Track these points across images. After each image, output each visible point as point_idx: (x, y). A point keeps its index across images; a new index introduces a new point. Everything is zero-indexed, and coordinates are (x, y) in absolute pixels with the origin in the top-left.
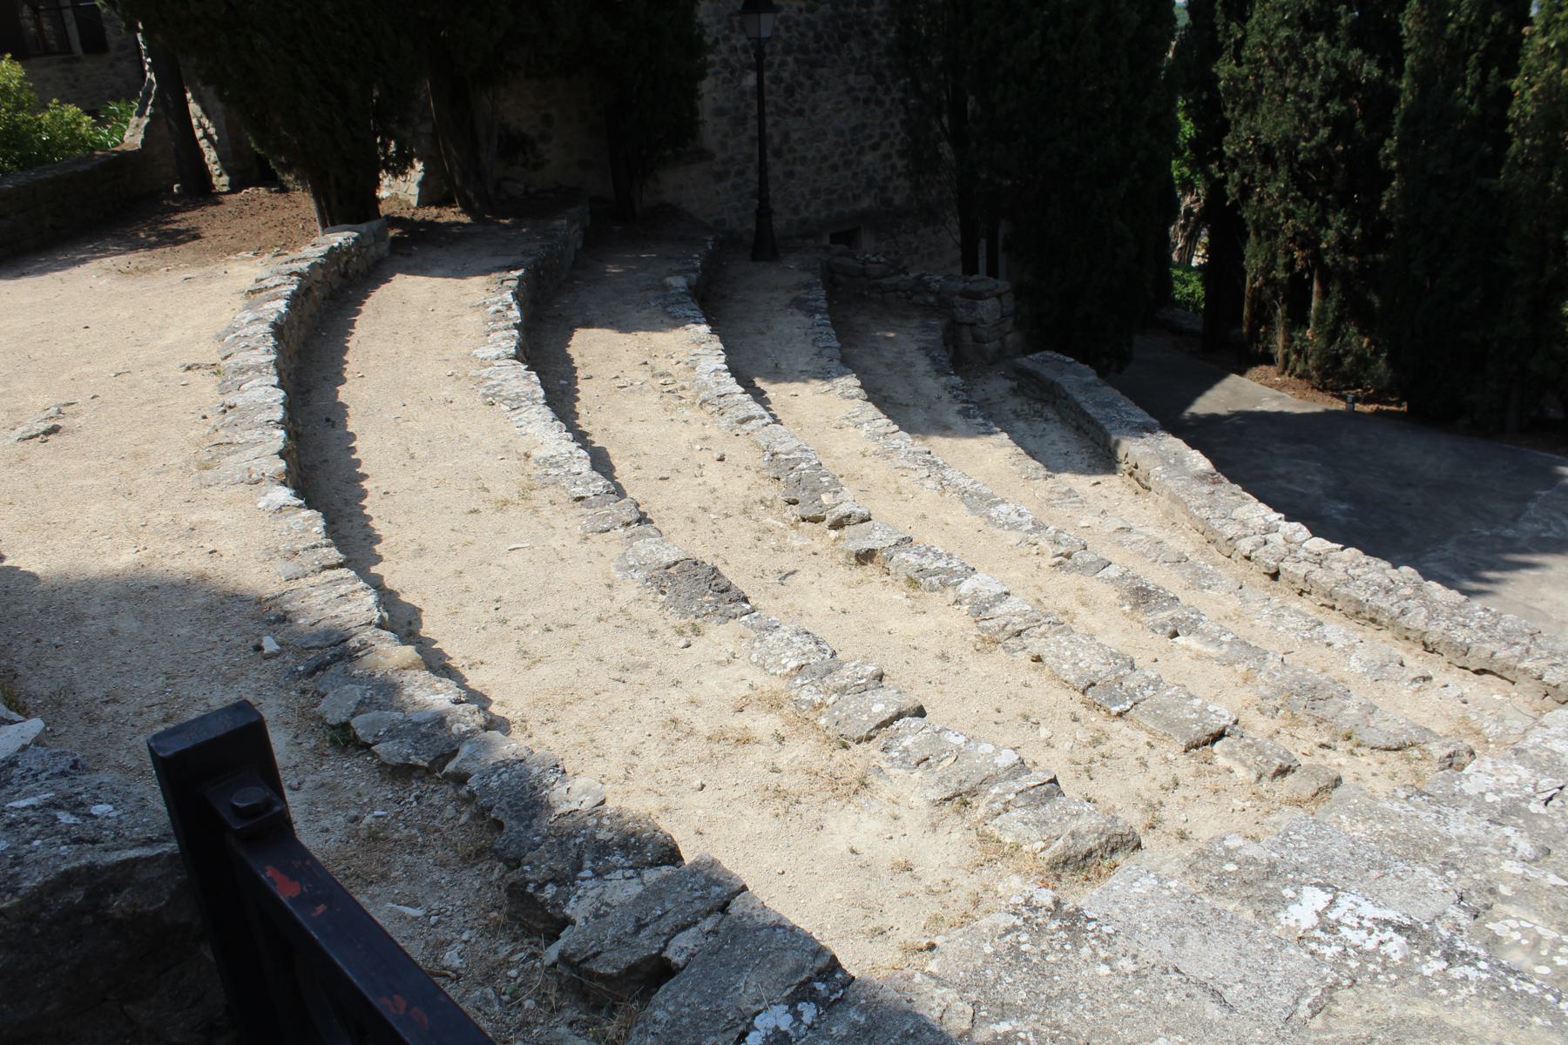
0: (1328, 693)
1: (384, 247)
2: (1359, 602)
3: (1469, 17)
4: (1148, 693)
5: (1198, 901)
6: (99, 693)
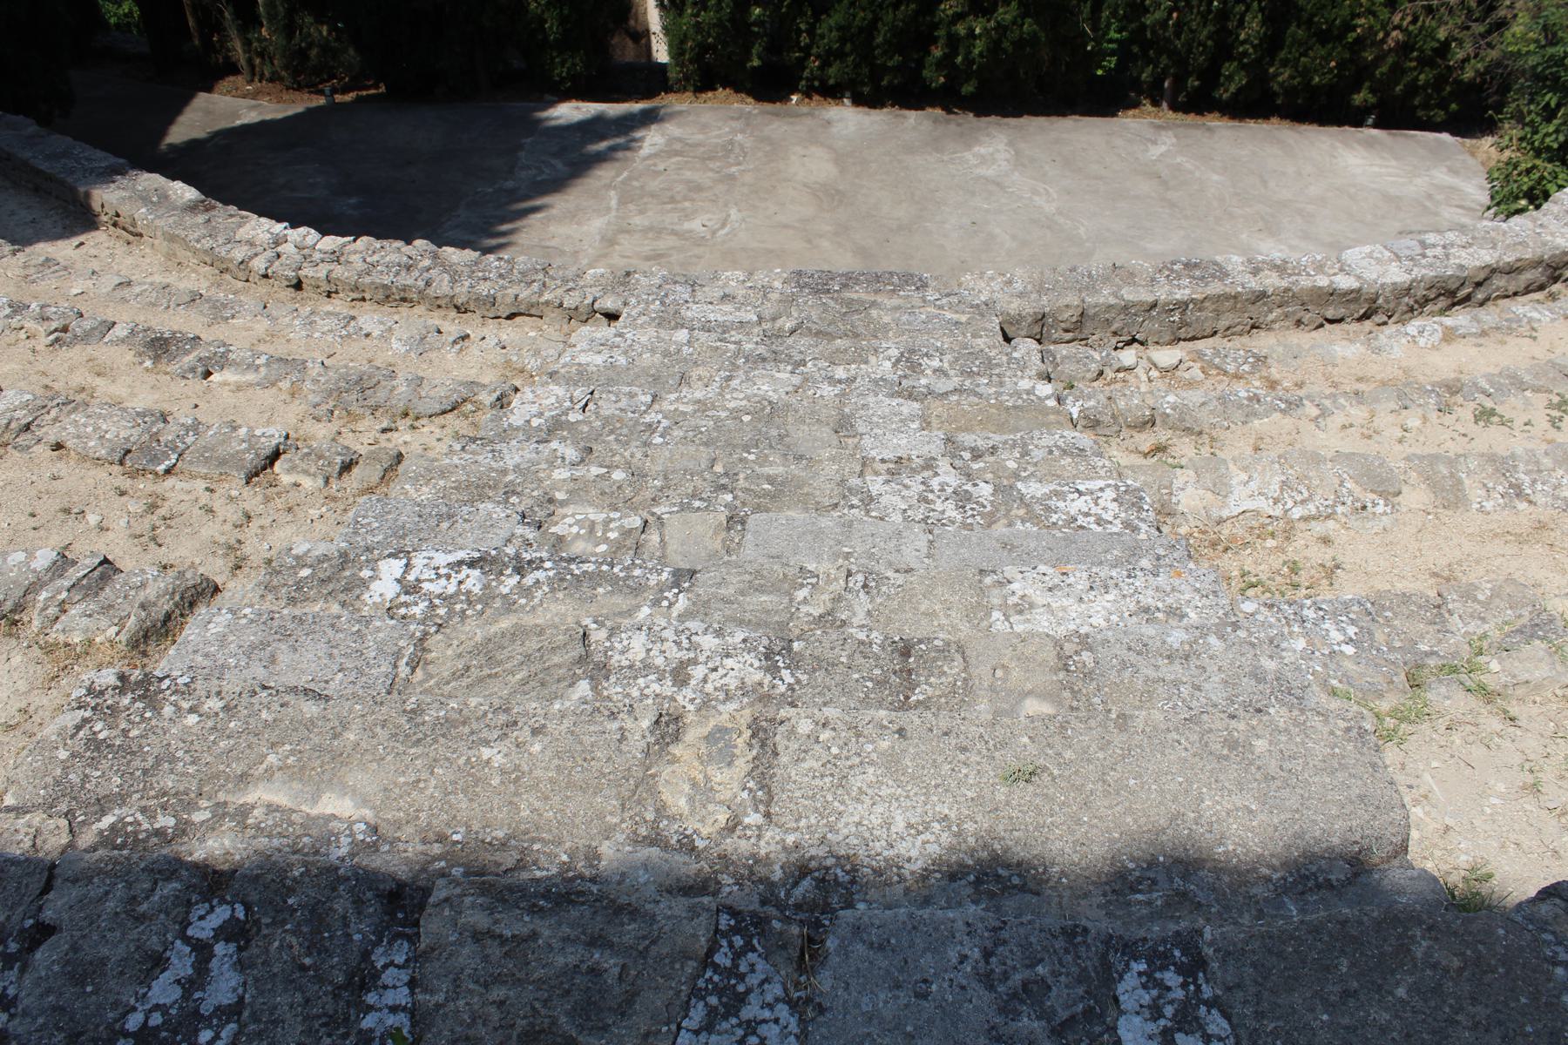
0: (374, 380)
2: (385, 286)
4: (190, 440)
5: (277, 615)
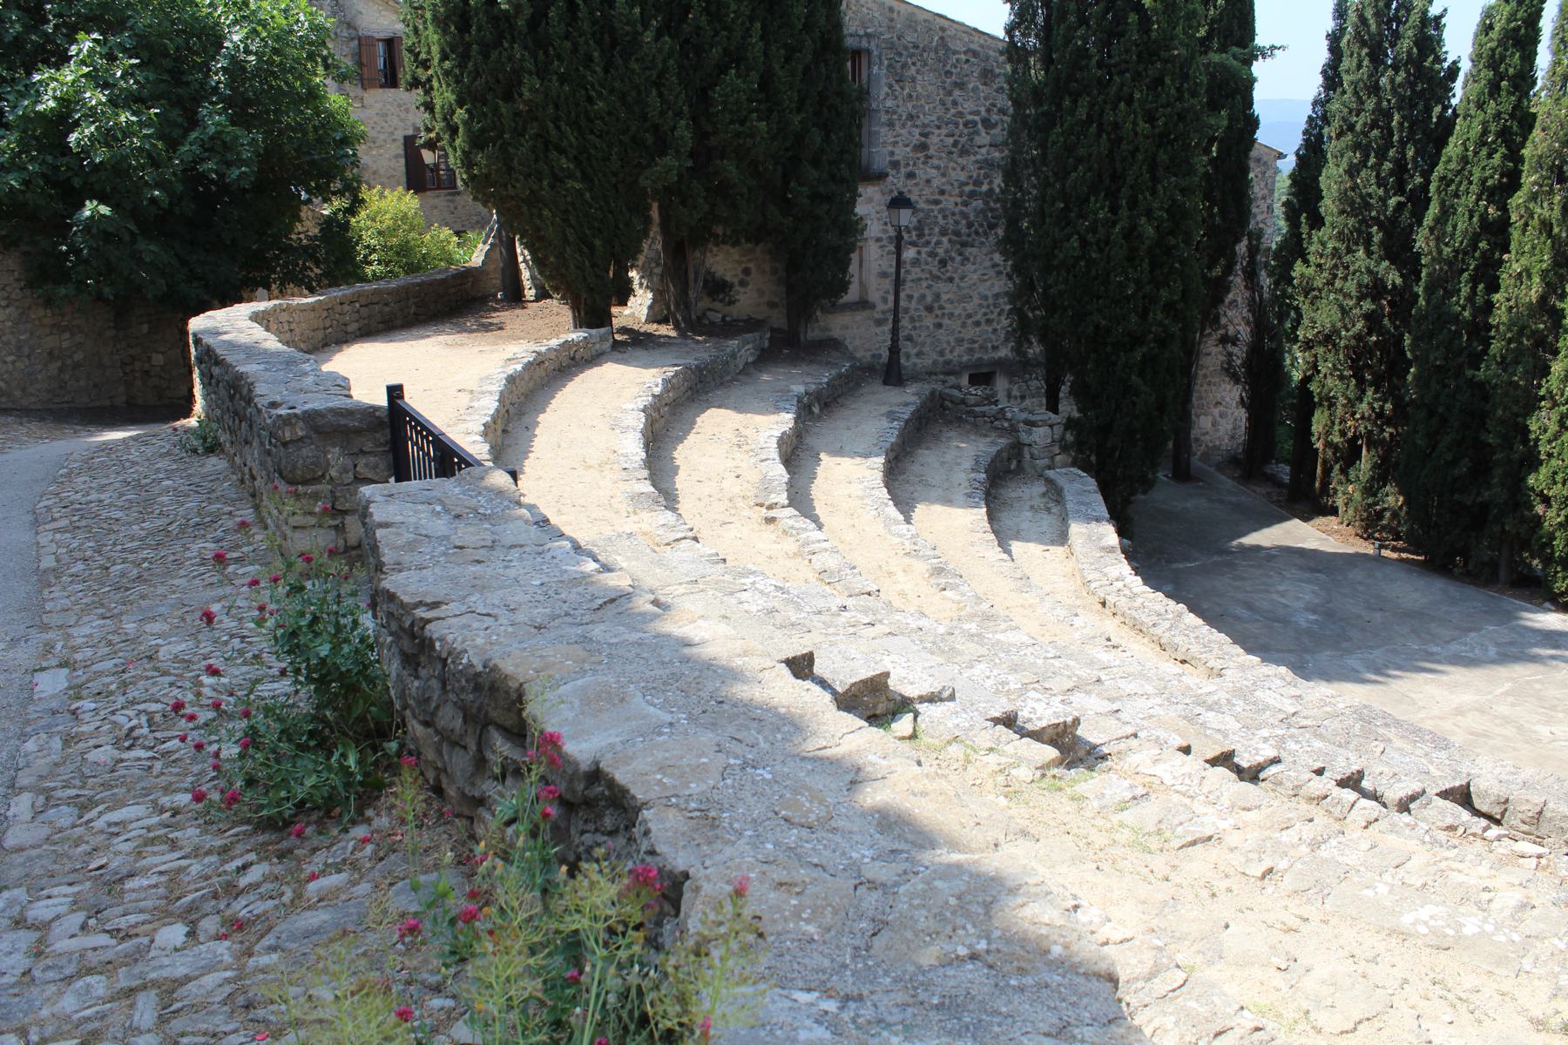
1: (607, 345)
3: (1462, 243)
6: (266, 402)
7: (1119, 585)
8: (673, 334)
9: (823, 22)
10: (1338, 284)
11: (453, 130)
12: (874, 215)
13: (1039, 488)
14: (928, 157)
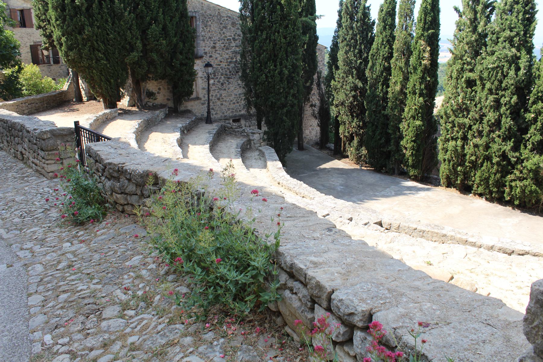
1: (117, 114)
7: (283, 178)
8: (137, 110)
9: (181, 8)
10: (344, 87)
11: (61, 45)
12: (199, 70)
13: (257, 153)
14: (216, 51)
